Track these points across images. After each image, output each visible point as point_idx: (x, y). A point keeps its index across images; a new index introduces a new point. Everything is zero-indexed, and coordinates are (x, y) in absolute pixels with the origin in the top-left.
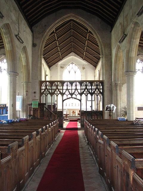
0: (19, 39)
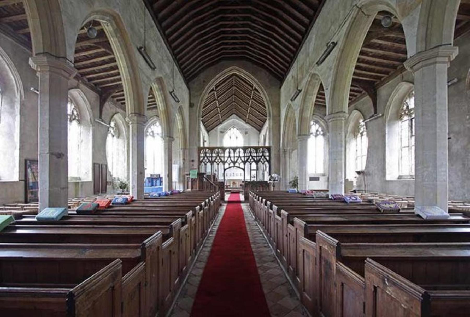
0: (174, 97)
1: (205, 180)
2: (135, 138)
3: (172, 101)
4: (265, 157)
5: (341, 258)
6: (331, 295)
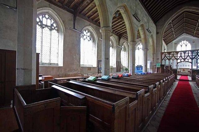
1: (165, 68)
2: (132, 51)
3: (148, 33)
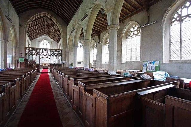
0: (9, 19)
4: (60, 54)
5: (86, 90)
6: (83, 103)
